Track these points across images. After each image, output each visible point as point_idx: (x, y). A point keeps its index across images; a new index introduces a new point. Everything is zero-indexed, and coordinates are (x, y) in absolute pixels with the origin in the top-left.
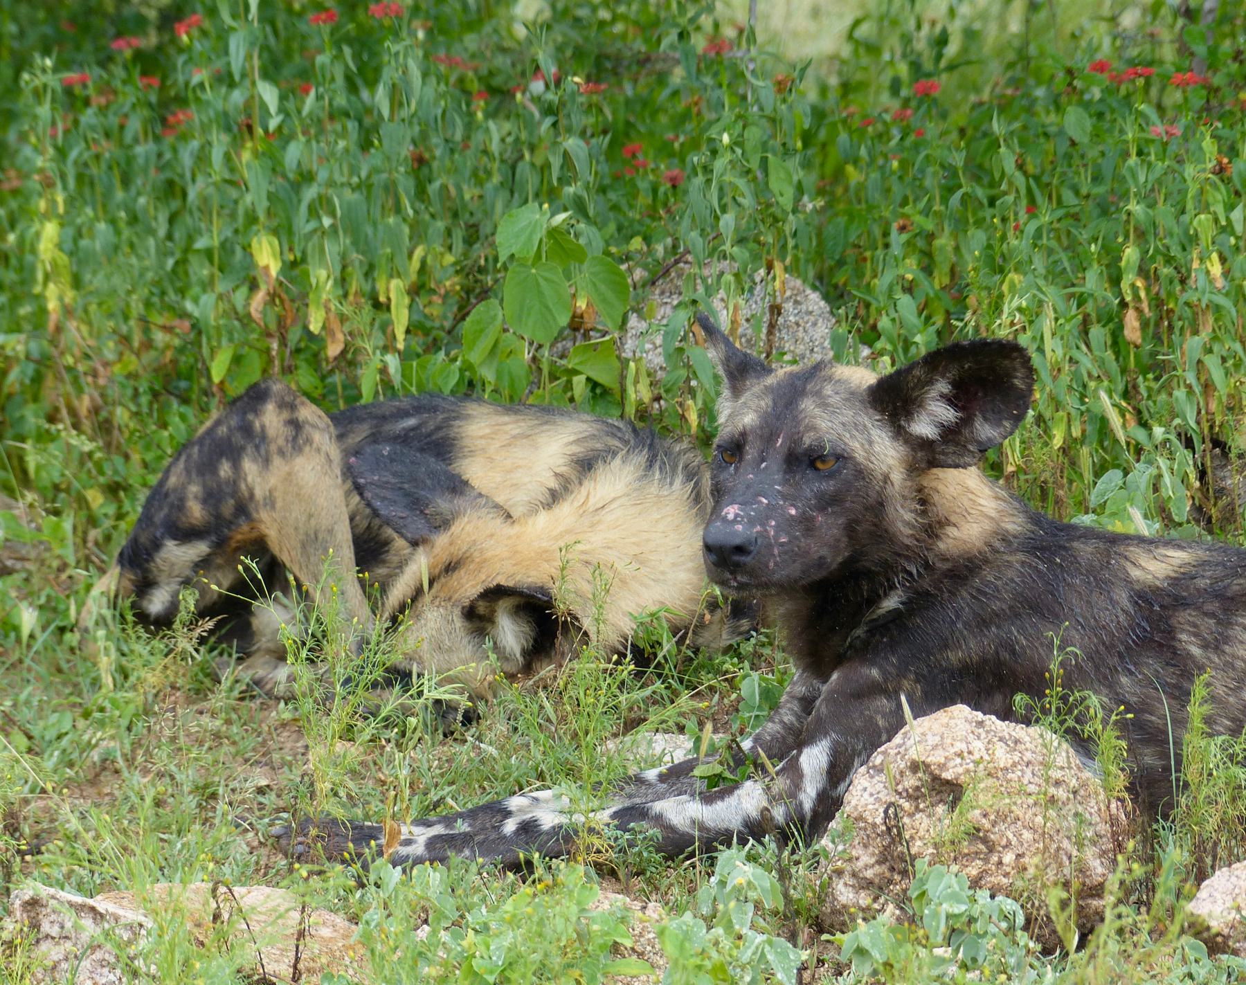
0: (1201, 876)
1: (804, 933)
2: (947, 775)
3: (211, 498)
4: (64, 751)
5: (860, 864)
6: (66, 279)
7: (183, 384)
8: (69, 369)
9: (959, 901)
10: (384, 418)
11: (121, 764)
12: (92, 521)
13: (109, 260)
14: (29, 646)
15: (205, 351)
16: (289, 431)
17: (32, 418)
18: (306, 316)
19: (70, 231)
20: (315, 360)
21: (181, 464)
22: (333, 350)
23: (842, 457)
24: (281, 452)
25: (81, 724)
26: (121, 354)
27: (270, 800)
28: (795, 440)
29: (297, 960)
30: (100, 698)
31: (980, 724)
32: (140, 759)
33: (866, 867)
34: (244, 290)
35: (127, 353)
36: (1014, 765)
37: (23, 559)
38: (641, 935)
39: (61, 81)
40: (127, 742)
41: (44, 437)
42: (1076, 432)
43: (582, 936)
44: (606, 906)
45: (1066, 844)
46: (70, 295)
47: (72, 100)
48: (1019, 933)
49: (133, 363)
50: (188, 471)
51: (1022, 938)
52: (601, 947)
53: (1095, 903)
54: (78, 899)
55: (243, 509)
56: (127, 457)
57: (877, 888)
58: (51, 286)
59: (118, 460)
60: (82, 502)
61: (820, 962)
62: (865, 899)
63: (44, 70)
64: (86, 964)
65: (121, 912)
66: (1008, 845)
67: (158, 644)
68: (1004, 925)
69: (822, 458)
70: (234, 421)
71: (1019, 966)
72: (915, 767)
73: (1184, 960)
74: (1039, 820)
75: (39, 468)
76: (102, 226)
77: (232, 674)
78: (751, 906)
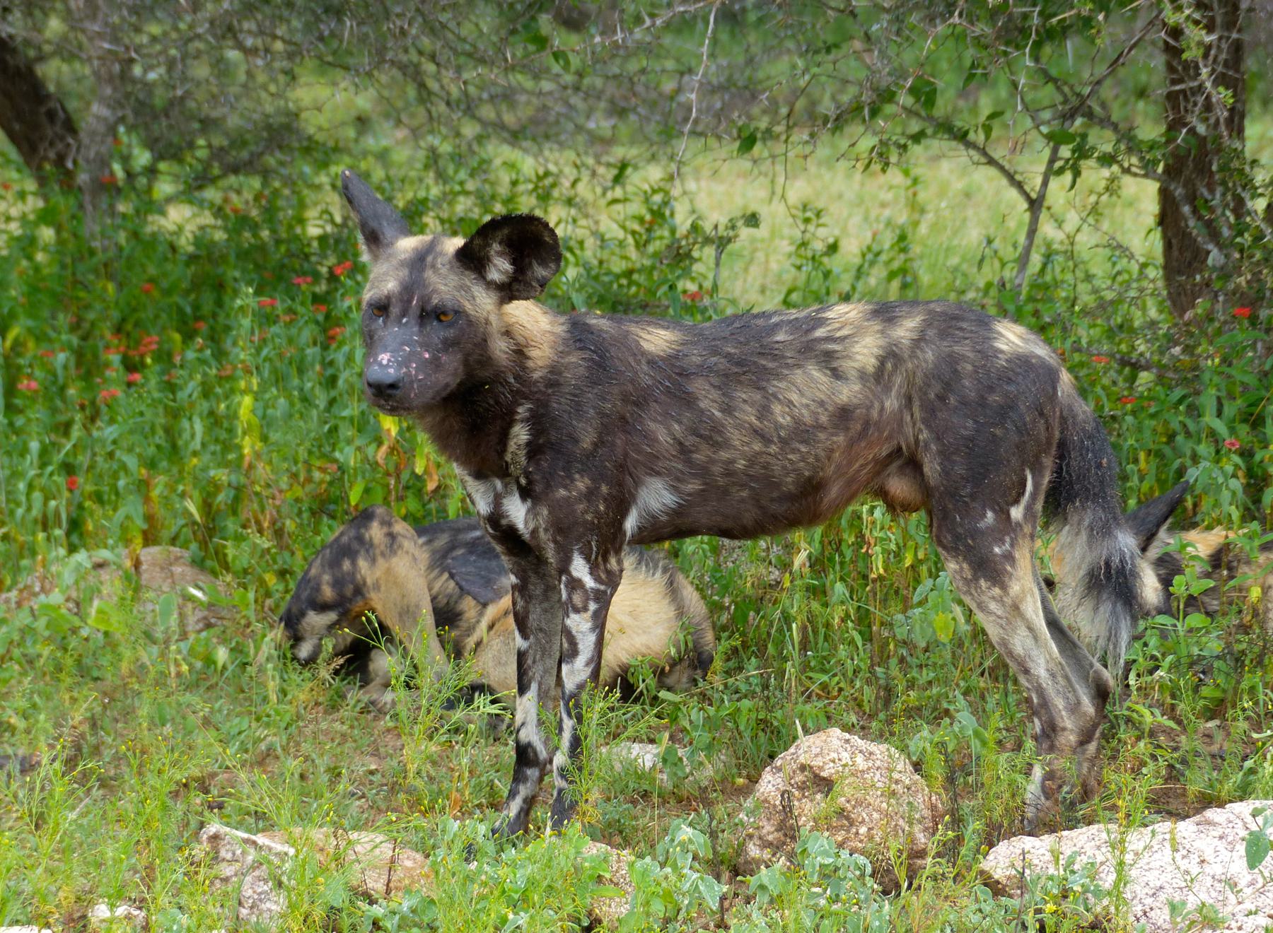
0: (991, 845)
1: (726, 875)
2: (824, 774)
3: (338, 583)
4: (242, 742)
5: (764, 831)
6: (256, 434)
7: (332, 507)
8: (257, 494)
9: (829, 856)
10: (459, 531)
11: (279, 750)
12: (268, 594)
13: (286, 423)
14: (222, 674)
15: (347, 485)
16: (387, 540)
17: (231, 525)
18: (414, 464)
19: (261, 404)
20: (419, 493)
21: (319, 561)
22: (431, 486)
23: (459, 312)
24: (383, 554)
25: (254, 724)
26: (291, 485)
27: (377, 778)
28: (425, 300)
29: (389, 881)
30: (267, 709)
31: (847, 741)
32: (292, 750)
33: (769, 833)
34: (374, 446)
35: (296, 485)
36: (869, 769)
37: (222, 618)
38: (617, 871)
39: (259, 303)
40: (284, 738)
41: (239, 538)
42: (921, 555)
43: (578, 869)
44: (595, 851)
45: (901, 822)
46: (259, 445)
47: (266, 319)
48: (867, 878)
49: (299, 492)
50: (323, 566)
51: (870, 882)
52: (590, 877)
53: (919, 862)
54: (246, 836)
55: (359, 591)
56: (293, 553)
57: (776, 847)
58: (247, 438)
59: (286, 554)
60: (262, 582)
61: (736, 895)
62: (767, 854)
63: (247, 295)
64: (248, 879)
65: (273, 845)
66: (863, 822)
67: (307, 674)
68: (858, 873)
69: (445, 313)
70: (352, 533)
71: (866, 900)
72: (803, 768)
73: (977, 900)
74: (884, 805)
75: (235, 557)
76: (282, 400)
77: (356, 696)
78: (690, 856)
